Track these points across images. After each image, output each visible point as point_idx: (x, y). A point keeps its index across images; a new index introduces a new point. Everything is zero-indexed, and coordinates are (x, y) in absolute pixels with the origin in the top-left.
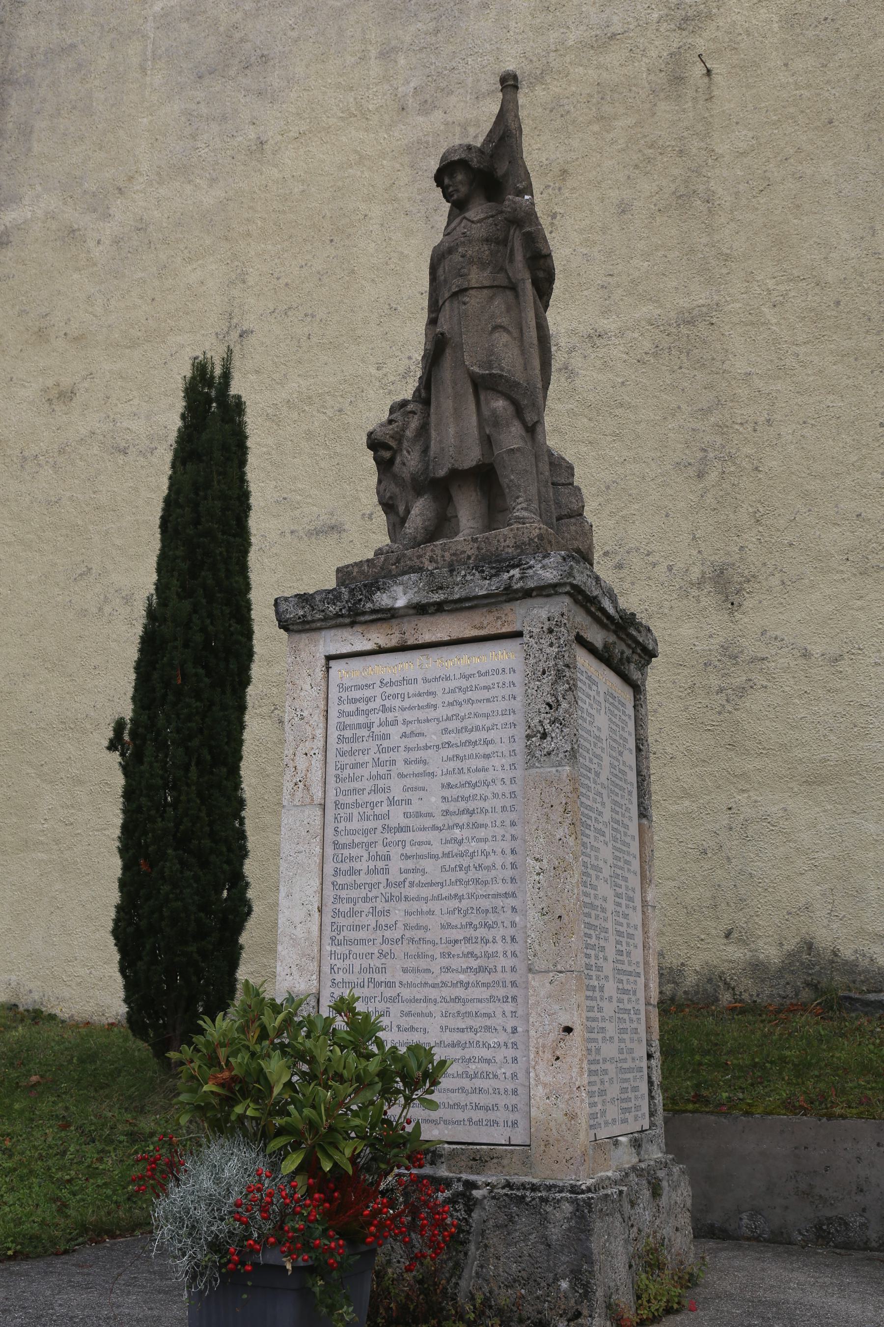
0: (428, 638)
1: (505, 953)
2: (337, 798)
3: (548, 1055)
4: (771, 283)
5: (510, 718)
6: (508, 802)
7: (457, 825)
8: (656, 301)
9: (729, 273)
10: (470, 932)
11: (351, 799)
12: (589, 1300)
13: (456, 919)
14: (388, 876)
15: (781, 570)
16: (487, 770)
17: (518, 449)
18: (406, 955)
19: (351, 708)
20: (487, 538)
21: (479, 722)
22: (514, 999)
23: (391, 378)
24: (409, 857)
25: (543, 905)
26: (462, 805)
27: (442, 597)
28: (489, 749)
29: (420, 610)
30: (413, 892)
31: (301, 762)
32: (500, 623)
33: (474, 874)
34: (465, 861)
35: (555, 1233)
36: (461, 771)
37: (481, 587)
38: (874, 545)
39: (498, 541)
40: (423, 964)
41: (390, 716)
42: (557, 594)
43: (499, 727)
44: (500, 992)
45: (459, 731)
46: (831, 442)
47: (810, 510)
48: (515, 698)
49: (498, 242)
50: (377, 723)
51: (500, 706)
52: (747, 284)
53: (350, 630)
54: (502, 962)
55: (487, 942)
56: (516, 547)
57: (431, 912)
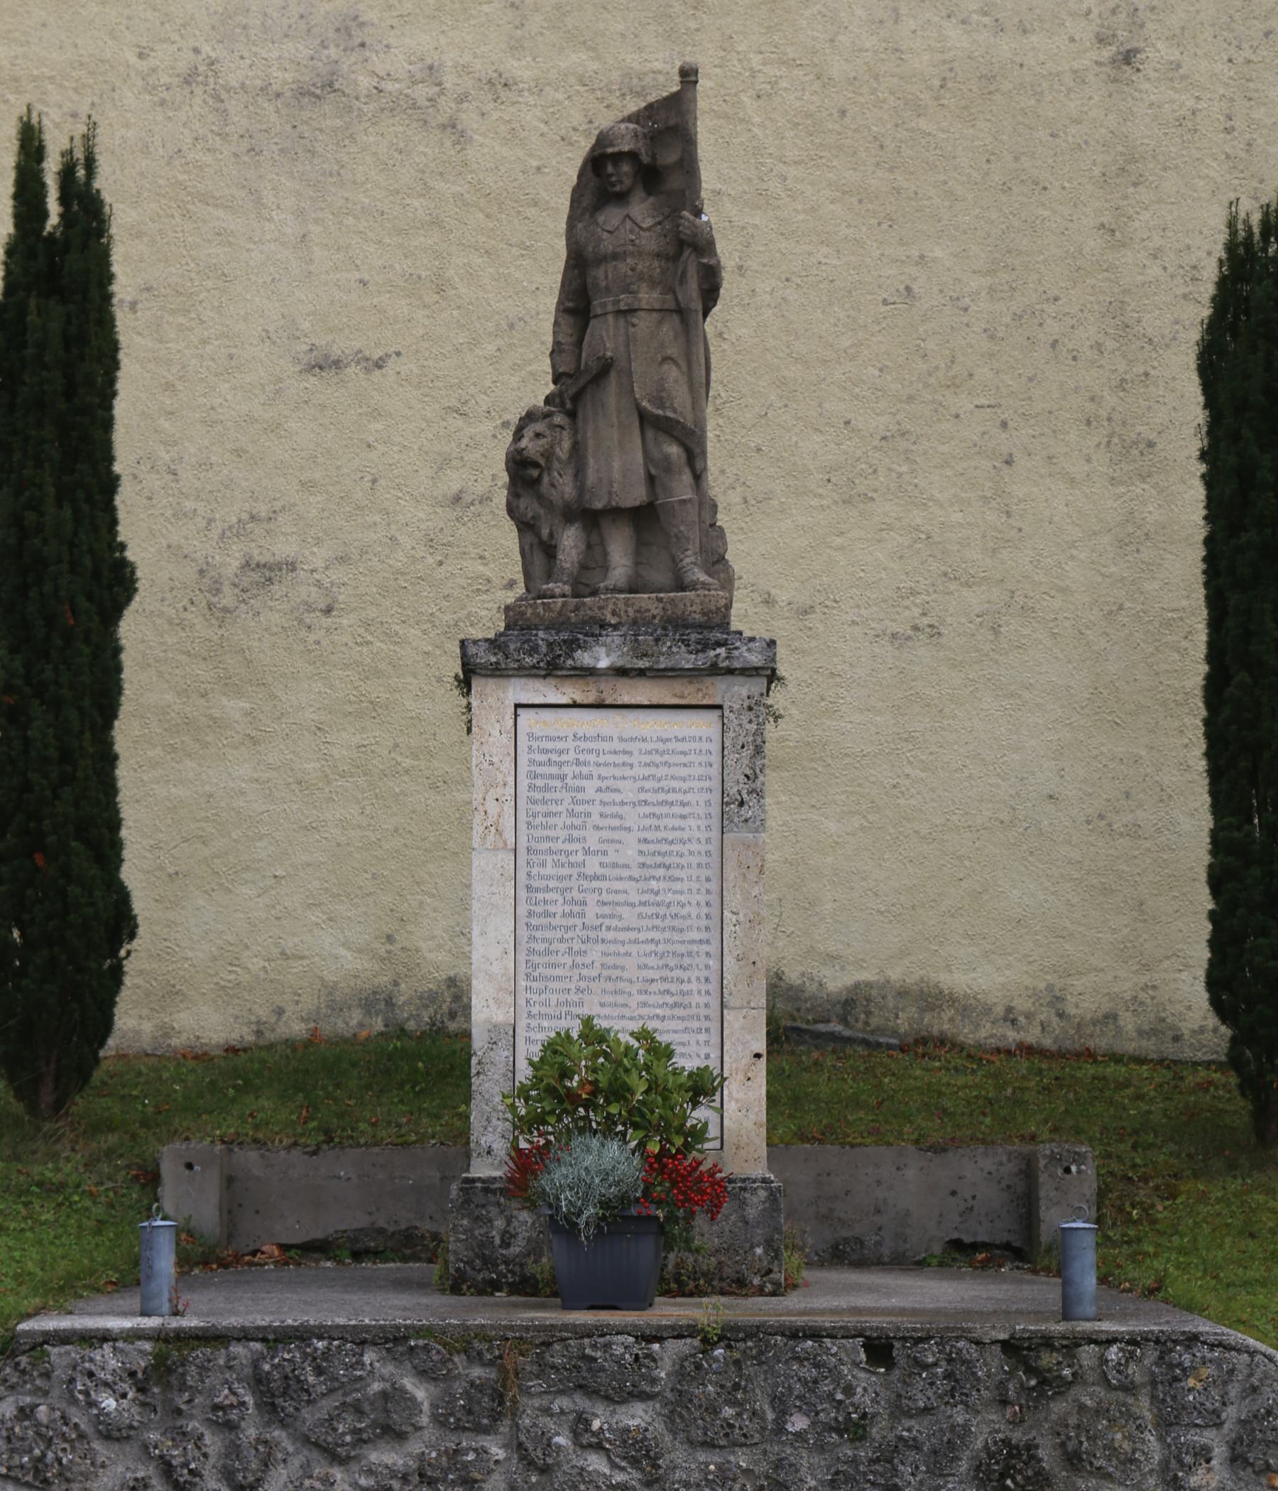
0: (626, 699)
1: (699, 992)
3: (741, 1077)
4: (756, 60)
5: (707, 784)
6: (704, 860)
7: (654, 878)
8: (593, 49)
9: (698, 30)
10: (666, 973)
11: (544, 846)
12: (780, 1261)
13: (652, 961)
16: (683, 829)
17: (690, 500)
18: (604, 991)
19: (543, 758)
21: (675, 784)
22: (707, 1030)
23: (165, 79)
26: (659, 859)
27: (647, 665)
28: (686, 810)
29: (620, 672)
30: (610, 935)
35: (752, 1213)
36: (657, 828)
37: (687, 660)
38: (863, 466)
40: (620, 999)
41: (585, 770)
42: (758, 675)
44: (695, 1024)
45: (656, 791)
46: (819, 314)
47: (786, 406)
49: (668, 259)
51: (699, 771)
52: (723, 53)
54: (696, 999)
55: (682, 982)
56: (704, 614)
57: (628, 954)
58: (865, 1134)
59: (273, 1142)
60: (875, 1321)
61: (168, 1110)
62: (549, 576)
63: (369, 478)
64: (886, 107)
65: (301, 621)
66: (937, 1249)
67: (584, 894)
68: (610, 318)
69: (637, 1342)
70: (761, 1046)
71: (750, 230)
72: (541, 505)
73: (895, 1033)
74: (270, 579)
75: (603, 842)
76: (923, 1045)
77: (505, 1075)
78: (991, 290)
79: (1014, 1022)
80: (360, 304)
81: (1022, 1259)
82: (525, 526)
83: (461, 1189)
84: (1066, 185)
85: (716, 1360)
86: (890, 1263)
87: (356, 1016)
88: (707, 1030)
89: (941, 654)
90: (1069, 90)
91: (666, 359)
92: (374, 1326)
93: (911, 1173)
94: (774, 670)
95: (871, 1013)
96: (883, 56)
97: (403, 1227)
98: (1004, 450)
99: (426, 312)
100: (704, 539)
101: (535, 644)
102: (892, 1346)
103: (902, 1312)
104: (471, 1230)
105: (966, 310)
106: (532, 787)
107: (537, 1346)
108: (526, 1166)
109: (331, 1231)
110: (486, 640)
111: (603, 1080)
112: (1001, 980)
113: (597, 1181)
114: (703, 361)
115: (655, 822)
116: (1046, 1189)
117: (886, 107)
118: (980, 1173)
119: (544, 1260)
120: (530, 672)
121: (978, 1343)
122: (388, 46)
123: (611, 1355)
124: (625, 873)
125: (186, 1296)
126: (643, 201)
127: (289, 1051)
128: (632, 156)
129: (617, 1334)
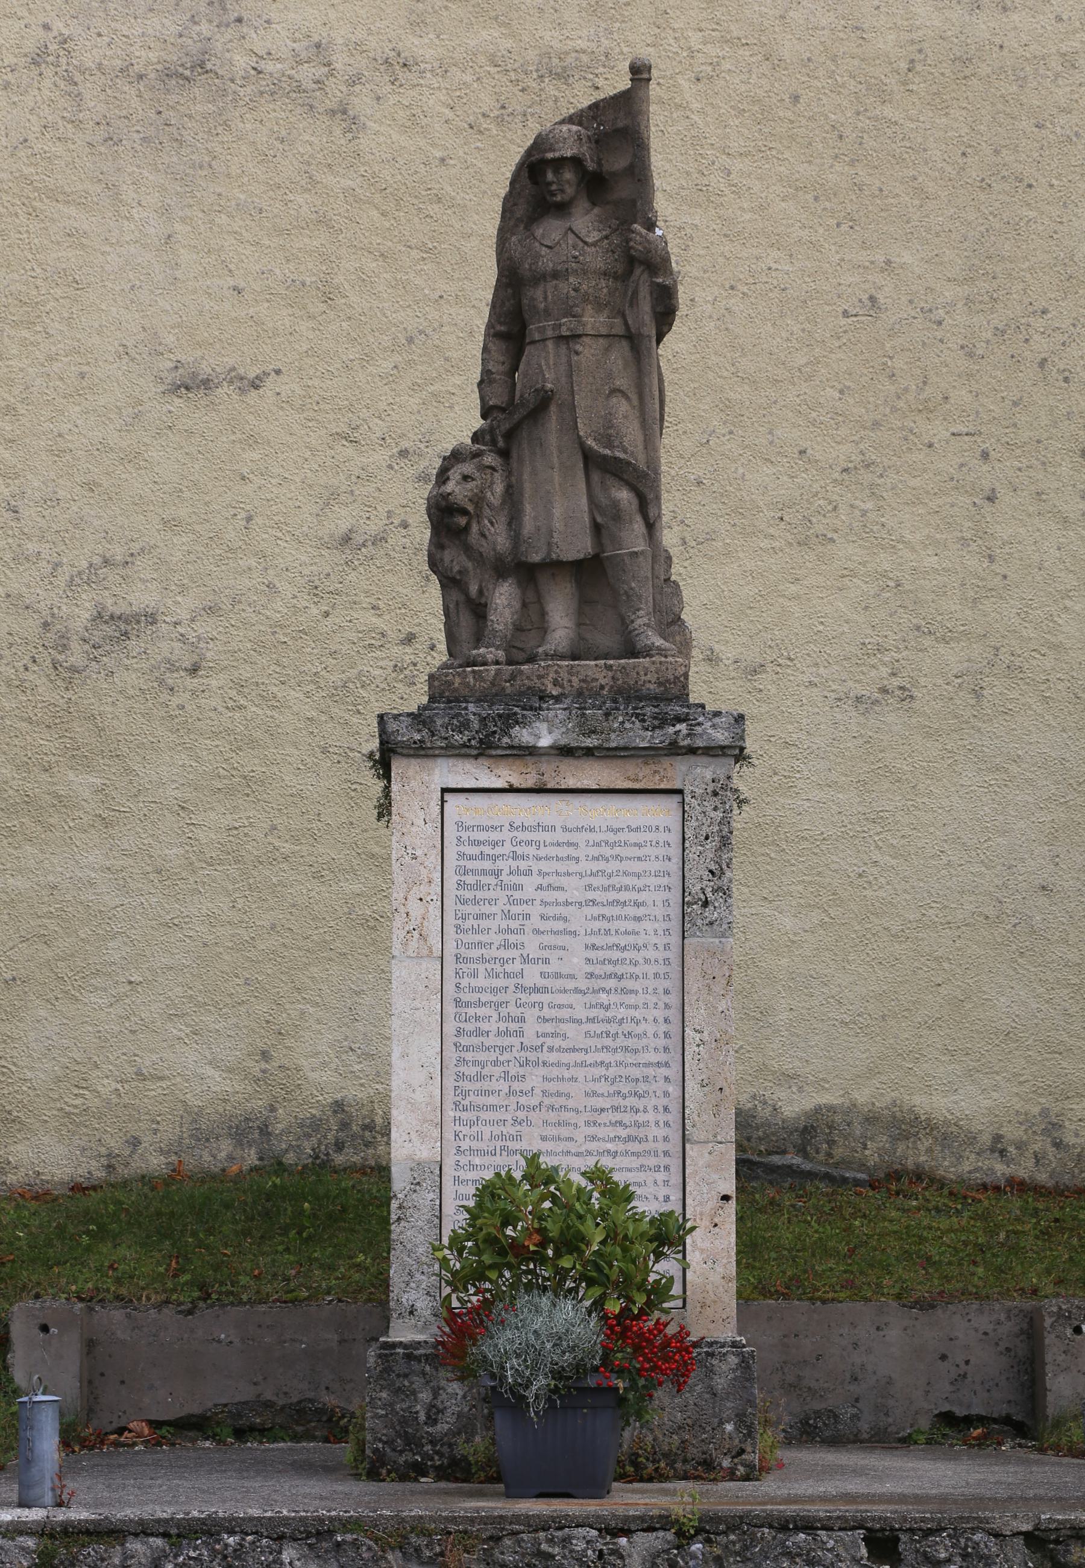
0: (571, 783)
1: (657, 1123)
2: (458, 951)
3: (705, 1223)
4: (695, 39)
5: (665, 881)
6: (662, 969)
7: (603, 990)
8: (507, 25)
10: (618, 1101)
11: (475, 953)
12: (753, 1439)
14: (522, 1040)
15: (682, 522)
16: (637, 933)
17: (642, 552)
18: (546, 1123)
19: (475, 850)
20: (623, 667)
22: (667, 1168)
24: (547, 1021)
25: (704, 1077)
26: (609, 969)
27: (596, 743)
28: (640, 912)
29: (565, 751)
30: (553, 1057)
31: (416, 909)
32: (657, 777)
33: (623, 1041)
34: (613, 1028)
35: (720, 1383)
36: (608, 932)
37: (642, 738)
38: (821, 502)
39: (638, 673)
40: (565, 1132)
41: (523, 865)
42: (724, 755)
43: (652, 888)
44: (652, 1161)
45: (606, 889)
46: (769, 327)
48: (670, 860)
49: (616, 277)
50: (506, 871)
51: (657, 866)
53: (474, 762)
54: (654, 1131)
56: (660, 684)
58: (838, 1288)
59: (139, 1299)
60: (878, 1510)
61: (13, 1261)
62: (478, 639)
63: (243, 515)
64: (846, 92)
65: (161, 682)
66: (924, 1423)
67: (521, 1010)
68: (550, 344)
69: (600, 1536)
70: (729, 1186)
71: (689, 231)
72: (469, 557)
73: (862, 1166)
74: (126, 634)
75: (544, 948)
76: (896, 1181)
77: (429, 1222)
78: (968, 301)
79: (1002, 1153)
80: (234, 314)
81: (1024, 1436)
82: (450, 582)
83: (380, 1356)
84: (1054, 182)
85: (694, 1556)
86: (869, 1441)
87: (225, 1147)
88: (667, 1168)
89: (914, 720)
90: (1057, 75)
91: (614, 391)
92: (294, 1518)
93: (894, 1333)
94: (742, 749)
95: (834, 1142)
96: (841, 35)
97: (295, 1400)
98: (986, 484)
99: (311, 324)
100: (658, 597)
101: (467, 716)
102: (897, 1540)
103: (902, 1499)
104: (391, 1405)
105: (940, 323)
106: (461, 885)
107: (484, 1541)
108: (462, 1332)
109: (210, 1404)
110: (409, 715)
111: (553, 1229)
112: (987, 1103)
113: (549, 1346)
114: (657, 393)
115: (605, 925)
116: (1053, 1353)
117: (846, 92)
118: (974, 1334)
119: (478, 1439)
120: (459, 752)
121: (997, 1535)
122: (268, 22)
123: (571, 1551)
124: (570, 985)
125: (71, 1485)
126: (588, 212)
127: (146, 1189)
128: (576, 162)
129: (577, 1526)
